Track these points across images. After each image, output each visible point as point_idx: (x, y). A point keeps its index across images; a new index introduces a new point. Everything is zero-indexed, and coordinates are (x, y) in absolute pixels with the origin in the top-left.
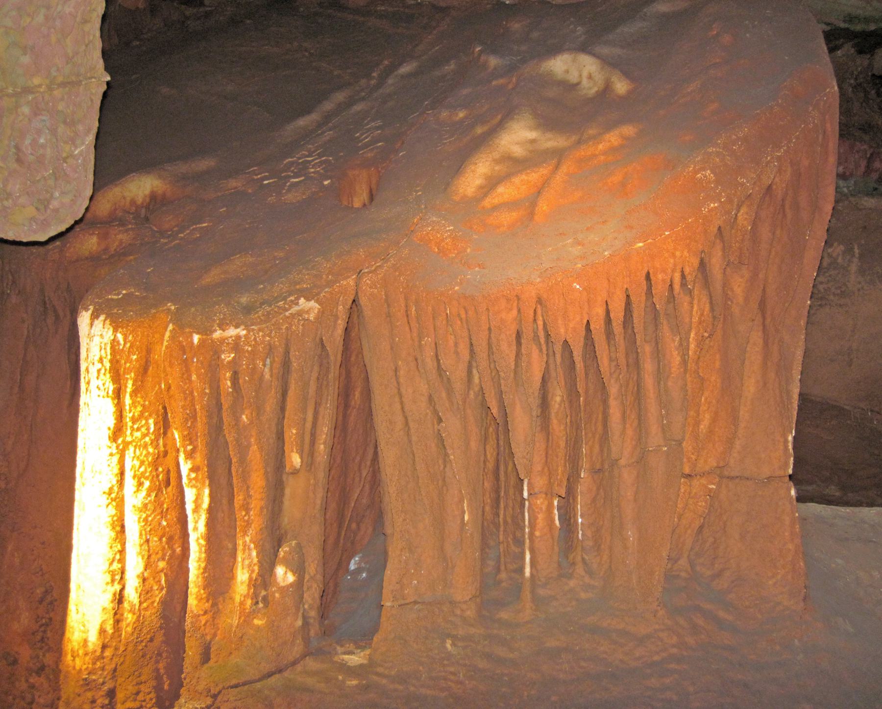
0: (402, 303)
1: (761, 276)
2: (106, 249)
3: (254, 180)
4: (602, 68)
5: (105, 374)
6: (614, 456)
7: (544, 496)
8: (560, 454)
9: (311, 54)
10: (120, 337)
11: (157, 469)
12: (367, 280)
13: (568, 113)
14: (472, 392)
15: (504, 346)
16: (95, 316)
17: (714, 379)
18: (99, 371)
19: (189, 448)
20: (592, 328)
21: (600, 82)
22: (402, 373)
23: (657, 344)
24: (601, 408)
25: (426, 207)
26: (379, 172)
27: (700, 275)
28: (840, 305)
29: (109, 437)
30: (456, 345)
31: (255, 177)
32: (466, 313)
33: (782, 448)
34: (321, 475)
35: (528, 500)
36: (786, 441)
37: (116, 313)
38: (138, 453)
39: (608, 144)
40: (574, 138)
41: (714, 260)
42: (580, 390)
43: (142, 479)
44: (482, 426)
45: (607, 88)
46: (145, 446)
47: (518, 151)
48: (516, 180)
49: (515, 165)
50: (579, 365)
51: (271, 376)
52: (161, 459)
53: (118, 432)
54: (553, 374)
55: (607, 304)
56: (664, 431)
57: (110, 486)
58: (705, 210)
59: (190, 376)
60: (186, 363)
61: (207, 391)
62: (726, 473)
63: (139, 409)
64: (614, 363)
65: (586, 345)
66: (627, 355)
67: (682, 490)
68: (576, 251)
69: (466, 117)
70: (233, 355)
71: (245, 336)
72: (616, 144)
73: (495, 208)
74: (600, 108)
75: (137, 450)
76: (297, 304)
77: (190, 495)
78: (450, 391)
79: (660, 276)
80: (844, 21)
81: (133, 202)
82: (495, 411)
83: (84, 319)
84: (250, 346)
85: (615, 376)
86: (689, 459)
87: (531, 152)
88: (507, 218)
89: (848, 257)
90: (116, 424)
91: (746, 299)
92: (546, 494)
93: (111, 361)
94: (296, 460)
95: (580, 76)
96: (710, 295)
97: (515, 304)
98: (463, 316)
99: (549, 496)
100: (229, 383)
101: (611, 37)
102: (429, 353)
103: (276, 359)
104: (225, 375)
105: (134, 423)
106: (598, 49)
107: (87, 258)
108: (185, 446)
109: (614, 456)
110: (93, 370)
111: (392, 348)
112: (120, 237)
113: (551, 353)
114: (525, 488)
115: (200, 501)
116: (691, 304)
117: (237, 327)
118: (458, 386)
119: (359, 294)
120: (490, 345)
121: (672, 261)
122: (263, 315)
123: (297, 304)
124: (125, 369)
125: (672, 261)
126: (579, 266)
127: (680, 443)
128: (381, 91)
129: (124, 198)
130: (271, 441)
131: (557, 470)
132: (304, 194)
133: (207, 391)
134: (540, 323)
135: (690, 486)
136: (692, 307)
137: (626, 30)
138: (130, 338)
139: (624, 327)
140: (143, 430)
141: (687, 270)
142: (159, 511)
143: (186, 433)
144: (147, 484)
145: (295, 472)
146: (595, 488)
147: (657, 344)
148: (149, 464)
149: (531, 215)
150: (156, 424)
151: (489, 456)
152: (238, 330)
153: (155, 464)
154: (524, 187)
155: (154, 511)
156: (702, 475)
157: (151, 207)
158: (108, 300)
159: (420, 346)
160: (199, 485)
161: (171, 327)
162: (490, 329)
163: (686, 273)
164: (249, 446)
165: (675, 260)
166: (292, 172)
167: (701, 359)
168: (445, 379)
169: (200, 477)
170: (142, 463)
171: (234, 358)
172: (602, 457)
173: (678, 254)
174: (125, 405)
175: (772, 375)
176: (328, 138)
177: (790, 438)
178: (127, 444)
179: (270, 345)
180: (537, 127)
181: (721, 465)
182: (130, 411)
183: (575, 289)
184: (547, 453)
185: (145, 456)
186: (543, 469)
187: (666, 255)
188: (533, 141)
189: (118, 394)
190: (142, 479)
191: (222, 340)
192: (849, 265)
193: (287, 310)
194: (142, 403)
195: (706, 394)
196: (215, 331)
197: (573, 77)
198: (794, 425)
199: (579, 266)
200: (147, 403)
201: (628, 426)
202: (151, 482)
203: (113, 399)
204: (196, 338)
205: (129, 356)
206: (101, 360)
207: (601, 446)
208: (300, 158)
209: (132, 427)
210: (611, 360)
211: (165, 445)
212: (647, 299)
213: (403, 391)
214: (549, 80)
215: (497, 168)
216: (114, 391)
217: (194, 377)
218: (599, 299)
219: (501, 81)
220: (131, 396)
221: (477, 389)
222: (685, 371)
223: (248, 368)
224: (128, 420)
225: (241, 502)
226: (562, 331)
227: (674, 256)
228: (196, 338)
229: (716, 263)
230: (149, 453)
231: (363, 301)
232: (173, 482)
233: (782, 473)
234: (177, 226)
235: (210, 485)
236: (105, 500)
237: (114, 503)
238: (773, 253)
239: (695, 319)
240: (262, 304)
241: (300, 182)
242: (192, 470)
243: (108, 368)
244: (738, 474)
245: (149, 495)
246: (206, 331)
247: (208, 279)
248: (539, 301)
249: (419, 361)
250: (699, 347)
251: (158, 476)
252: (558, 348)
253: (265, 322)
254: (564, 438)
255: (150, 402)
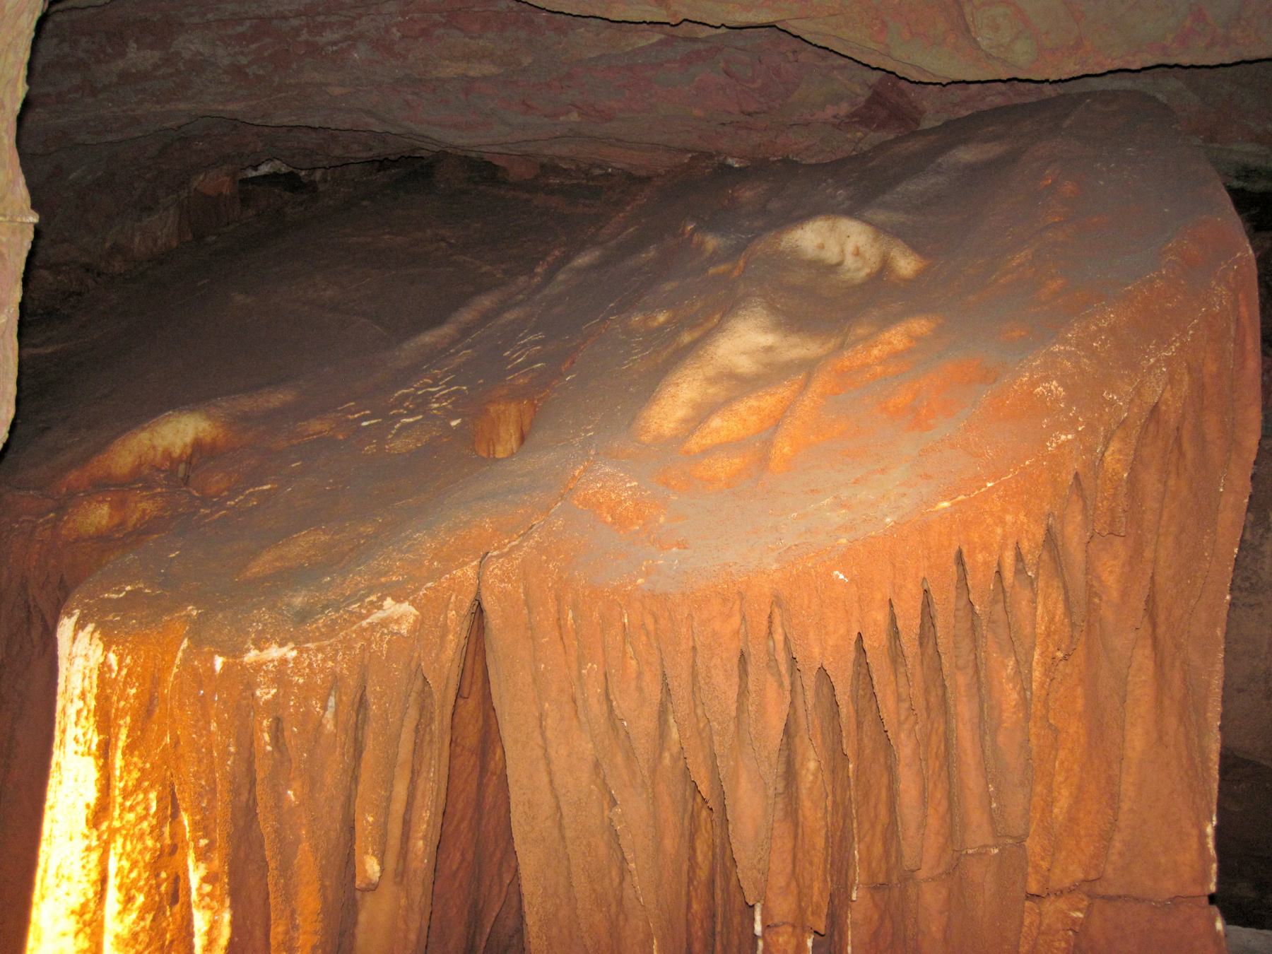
0: (552, 607)
1: (1148, 554)
2: (123, 523)
3: (348, 420)
4: (875, 240)
5: (87, 718)
6: (908, 863)
7: (790, 929)
8: (816, 860)
9: (450, 245)
10: (113, 659)
11: (158, 875)
12: (494, 569)
13: (820, 304)
14: (667, 755)
15: (718, 677)
16: (80, 626)
17: (1074, 729)
18: (79, 712)
19: (203, 842)
20: (866, 647)
21: (873, 259)
22: (549, 722)
23: (977, 671)
24: (885, 780)
25: (597, 454)
26: (535, 406)
27: (1045, 556)
28: (1251, 606)
29: (87, 820)
30: (639, 675)
31: (351, 417)
32: (656, 622)
33: (1195, 846)
34: (417, 892)
35: (763, 937)
36: (1202, 836)
37: (111, 621)
38: (129, 847)
39: (887, 348)
40: (833, 343)
41: (1069, 529)
42: (848, 752)
43: (133, 892)
44: (685, 810)
45: (885, 266)
46: (141, 837)
47: (745, 365)
48: (741, 407)
49: (740, 385)
50: (846, 710)
51: (336, 726)
52: (165, 859)
53: (100, 813)
54: (803, 722)
55: (891, 606)
56: (992, 821)
57: (82, 900)
58: (1051, 447)
59: (209, 723)
60: (203, 702)
61: (232, 749)
62: (1099, 890)
63: (136, 774)
64: (907, 705)
65: (857, 674)
66: (927, 691)
67: (1027, 922)
68: (838, 517)
69: (668, 322)
70: (274, 691)
71: (295, 659)
72: (900, 346)
73: (706, 452)
74: (877, 295)
75: (128, 843)
76: (380, 608)
77: (201, 921)
78: (630, 755)
79: (980, 557)
80: (1237, 178)
81: (167, 454)
82: (703, 788)
83: (66, 628)
84: (302, 675)
85: (906, 726)
86: (1036, 866)
87: (765, 365)
88: (724, 466)
89: (1260, 531)
90: (98, 799)
91: (1124, 594)
92: (794, 926)
93: (97, 698)
94: (372, 867)
95: (843, 251)
96: (1065, 587)
97: (737, 607)
98: (651, 627)
99: (798, 930)
100: (267, 737)
101: (887, 197)
102: (595, 690)
103: (344, 698)
104: (261, 723)
105: (125, 798)
106: (868, 214)
107: (91, 538)
108: (196, 840)
109: (908, 863)
110: (72, 712)
111: (534, 680)
112: (143, 505)
113: (799, 689)
114: (758, 918)
115: (215, 932)
116: (1033, 601)
117: (281, 645)
118: (643, 746)
119: (483, 591)
120: (694, 674)
121: (999, 530)
122: (325, 625)
123: (380, 608)
124: (117, 709)
125: (999, 530)
126: (844, 541)
127: (1020, 841)
128: (546, 292)
129: (154, 448)
130: (333, 835)
131: (810, 887)
132: (418, 440)
133: (232, 749)
134: (779, 637)
135: (1040, 914)
136: (1036, 608)
137: (912, 187)
138: (128, 660)
139: (921, 644)
140: (140, 809)
141: (1025, 546)
142: (157, 945)
143: (198, 817)
144: (140, 899)
145: (372, 888)
146: (876, 917)
147: (977, 671)
148: (145, 867)
149: (764, 460)
150: (159, 800)
151: (700, 858)
152: (285, 649)
153: (154, 867)
154: (754, 418)
155: (148, 945)
156: (1060, 893)
157: (194, 461)
158: (104, 600)
159: (580, 676)
160: (215, 904)
161: (185, 643)
162: (694, 648)
163: (1023, 552)
164: (298, 841)
165: (1008, 529)
166: (406, 408)
167: (1051, 696)
168: (622, 733)
169: (218, 892)
170: (134, 864)
171: (275, 696)
172: (887, 863)
173: (1009, 518)
174: (113, 768)
175: (1172, 722)
176: (464, 359)
177: (1210, 830)
178: (113, 832)
179: (333, 673)
180: (775, 328)
181: (1090, 878)
182: (121, 778)
183: (836, 582)
184: (795, 857)
185: (141, 853)
186: (788, 885)
187: (989, 521)
188: (769, 349)
189: (105, 751)
190: (133, 892)
191: (258, 667)
192: (1261, 545)
193: (367, 616)
194: (140, 765)
195: (1062, 754)
196: (248, 650)
197: (831, 255)
198: (1214, 808)
199: (844, 541)
200: (148, 765)
201: (931, 811)
202: (148, 895)
203: (97, 758)
204: (219, 662)
205: (125, 690)
206: (83, 696)
207: (885, 844)
208: (418, 389)
209: (122, 805)
210: (899, 699)
211: (173, 836)
212: (958, 597)
213: (552, 752)
214: (797, 260)
215: (711, 391)
216: (99, 745)
217: (213, 727)
218: (879, 596)
219: (723, 268)
220: (124, 754)
221: (675, 749)
222: (1027, 718)
223: (297, 712)
224: (117, 792)
225: (280, 937)
226: (816, 651)
227: (1002, 521)
228: (219, 662)
229: (1073, 535)
230: (146, 848)
231: (489, 604)
232: (181, 899)
233: (1197, 890)
234: (228, 489)
235: (231, 907)
236: (72, 924)
237: (88, 930)
238: (1165, 518)
239: (1041, 629)
240: (325, 607)
241: (415, 422)
242: (205, 880)
243: (92, 707)
244: (1121, 893)
245: (141, 918)
246: (234, 651)
247: (257, 568)
248: (777, 601)
249: (580, 703)
250: (1047, 676)
251: (159, 886)
252: (809, 680)
253: (328, 636)
254: (823, 833)
255: (152, 764)
